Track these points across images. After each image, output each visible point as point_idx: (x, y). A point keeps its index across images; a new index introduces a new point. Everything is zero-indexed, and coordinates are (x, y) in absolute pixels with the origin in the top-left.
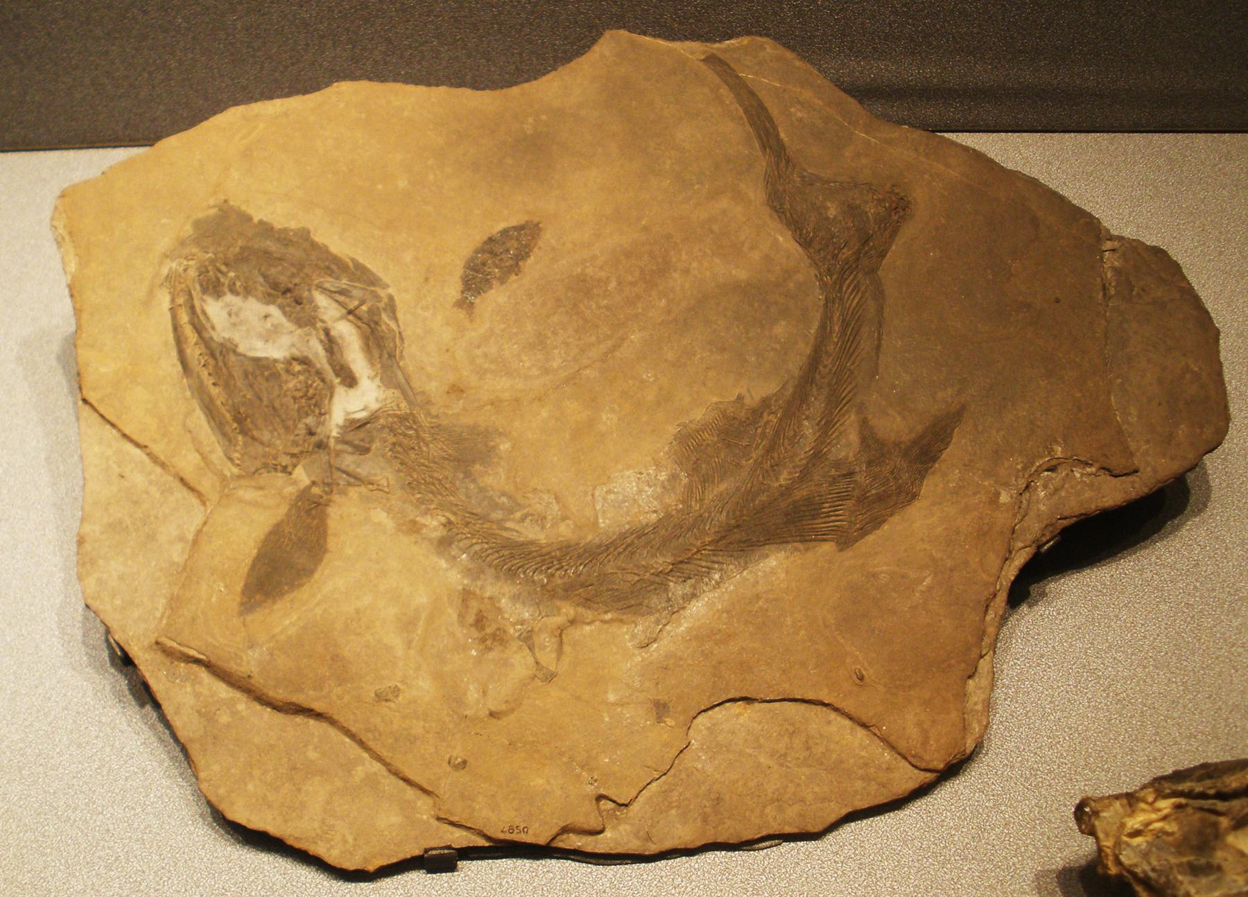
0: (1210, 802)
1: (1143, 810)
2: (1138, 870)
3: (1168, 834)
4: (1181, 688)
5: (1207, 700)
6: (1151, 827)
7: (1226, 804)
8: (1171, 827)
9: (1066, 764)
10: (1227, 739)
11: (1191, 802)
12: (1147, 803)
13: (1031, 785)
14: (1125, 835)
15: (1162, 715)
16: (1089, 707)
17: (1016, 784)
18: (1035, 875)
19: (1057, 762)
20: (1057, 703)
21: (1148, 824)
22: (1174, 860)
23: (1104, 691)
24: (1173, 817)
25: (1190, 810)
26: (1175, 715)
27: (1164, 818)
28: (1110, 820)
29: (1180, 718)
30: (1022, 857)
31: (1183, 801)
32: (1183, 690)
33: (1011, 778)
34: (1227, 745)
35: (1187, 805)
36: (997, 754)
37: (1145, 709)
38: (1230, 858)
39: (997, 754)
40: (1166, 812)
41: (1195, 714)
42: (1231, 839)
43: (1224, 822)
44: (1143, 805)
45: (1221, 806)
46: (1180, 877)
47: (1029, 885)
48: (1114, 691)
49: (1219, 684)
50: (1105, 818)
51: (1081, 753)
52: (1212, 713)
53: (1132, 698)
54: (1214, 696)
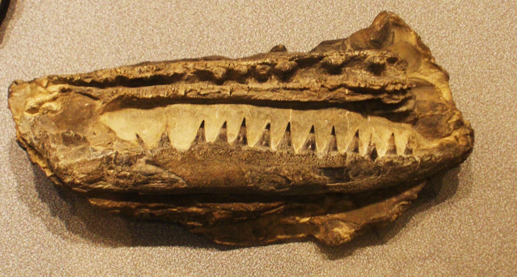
0: (89, 88)
1: (40, 92)
2: (27, 138)
3: (53, 112)
4: (174, 6)
5: (192, 16)
6: (44, 106)
7: (101, 90)
8: (55, 106)
9: (62, 58)
10: (198, 46)
11: (73, 87)
12: (42, 87)
13: (29, 72)
14: (26, 111)
15: (150, 25)
16: (95, 16)
17: (18, 71)
18: (11, 140)
19: (56, 56)
20: (70, 12)
21: (41, 104)
22: (52, 131)
23: (111, 4)
24: (60, 99)
25: (72, 93)
26: (162, 26)
27: (54, 99)
28: (19, 99)
29: (165, 28)
30: (5, 125)
31: (67, 86)
32: (175, 7)
33: (16, 66)
34: (196, 51)
35: (69, 90)
36: (10, 48)
37: (139, 20)
38: (99, 133)
39: (10, 48)
40: (55, 94)
41: (177, 26)
42: (105, 119)
43: (99, 105)
44: (40, 89)
45: (95, 91)
46: (53, 145)
47: (4, 147)
48: (118, 5)
49: (206, 4)
50: (15, 97)
51: (76, 51)
52: (192, 26)
53: (132, 11)
54: (199, 13)
